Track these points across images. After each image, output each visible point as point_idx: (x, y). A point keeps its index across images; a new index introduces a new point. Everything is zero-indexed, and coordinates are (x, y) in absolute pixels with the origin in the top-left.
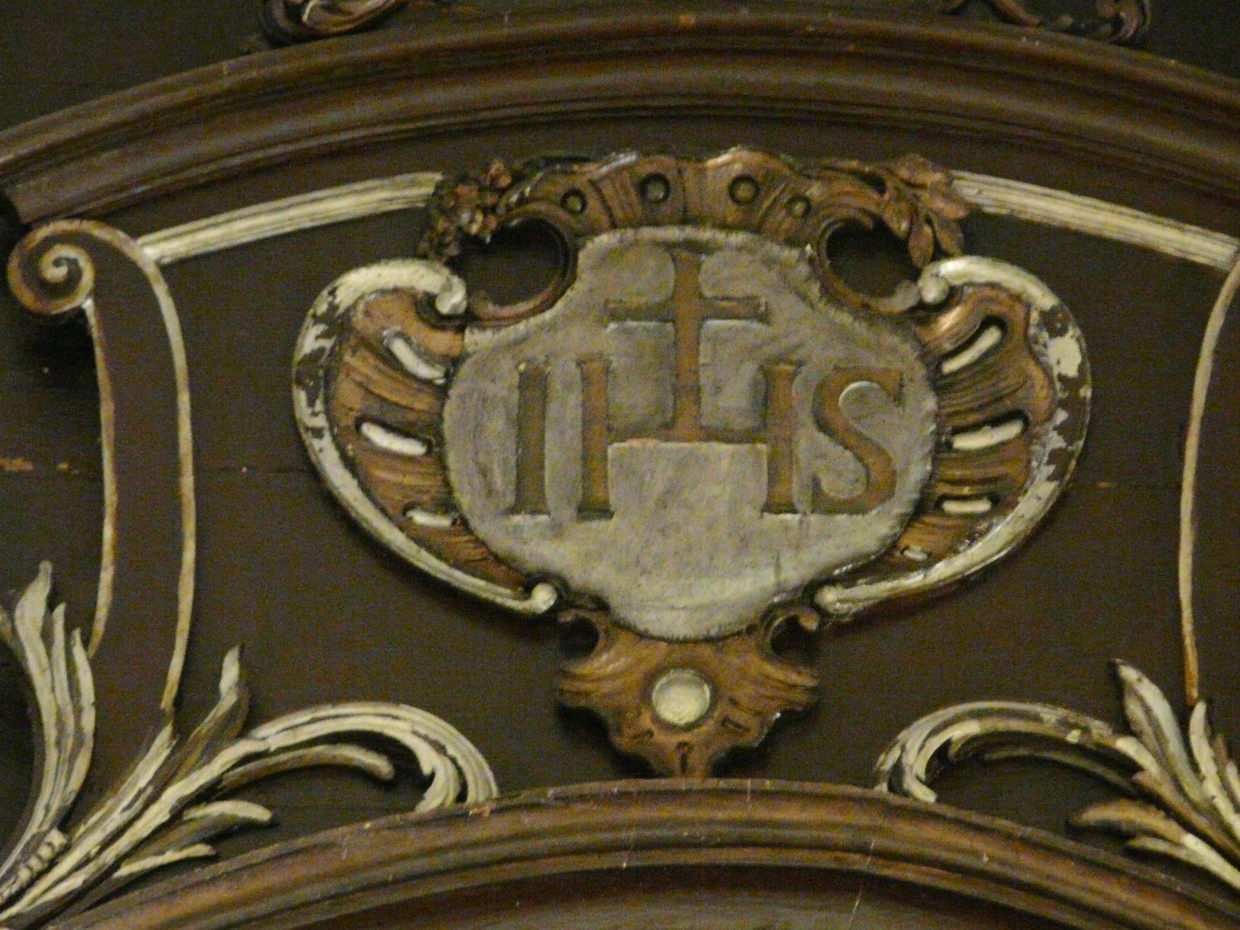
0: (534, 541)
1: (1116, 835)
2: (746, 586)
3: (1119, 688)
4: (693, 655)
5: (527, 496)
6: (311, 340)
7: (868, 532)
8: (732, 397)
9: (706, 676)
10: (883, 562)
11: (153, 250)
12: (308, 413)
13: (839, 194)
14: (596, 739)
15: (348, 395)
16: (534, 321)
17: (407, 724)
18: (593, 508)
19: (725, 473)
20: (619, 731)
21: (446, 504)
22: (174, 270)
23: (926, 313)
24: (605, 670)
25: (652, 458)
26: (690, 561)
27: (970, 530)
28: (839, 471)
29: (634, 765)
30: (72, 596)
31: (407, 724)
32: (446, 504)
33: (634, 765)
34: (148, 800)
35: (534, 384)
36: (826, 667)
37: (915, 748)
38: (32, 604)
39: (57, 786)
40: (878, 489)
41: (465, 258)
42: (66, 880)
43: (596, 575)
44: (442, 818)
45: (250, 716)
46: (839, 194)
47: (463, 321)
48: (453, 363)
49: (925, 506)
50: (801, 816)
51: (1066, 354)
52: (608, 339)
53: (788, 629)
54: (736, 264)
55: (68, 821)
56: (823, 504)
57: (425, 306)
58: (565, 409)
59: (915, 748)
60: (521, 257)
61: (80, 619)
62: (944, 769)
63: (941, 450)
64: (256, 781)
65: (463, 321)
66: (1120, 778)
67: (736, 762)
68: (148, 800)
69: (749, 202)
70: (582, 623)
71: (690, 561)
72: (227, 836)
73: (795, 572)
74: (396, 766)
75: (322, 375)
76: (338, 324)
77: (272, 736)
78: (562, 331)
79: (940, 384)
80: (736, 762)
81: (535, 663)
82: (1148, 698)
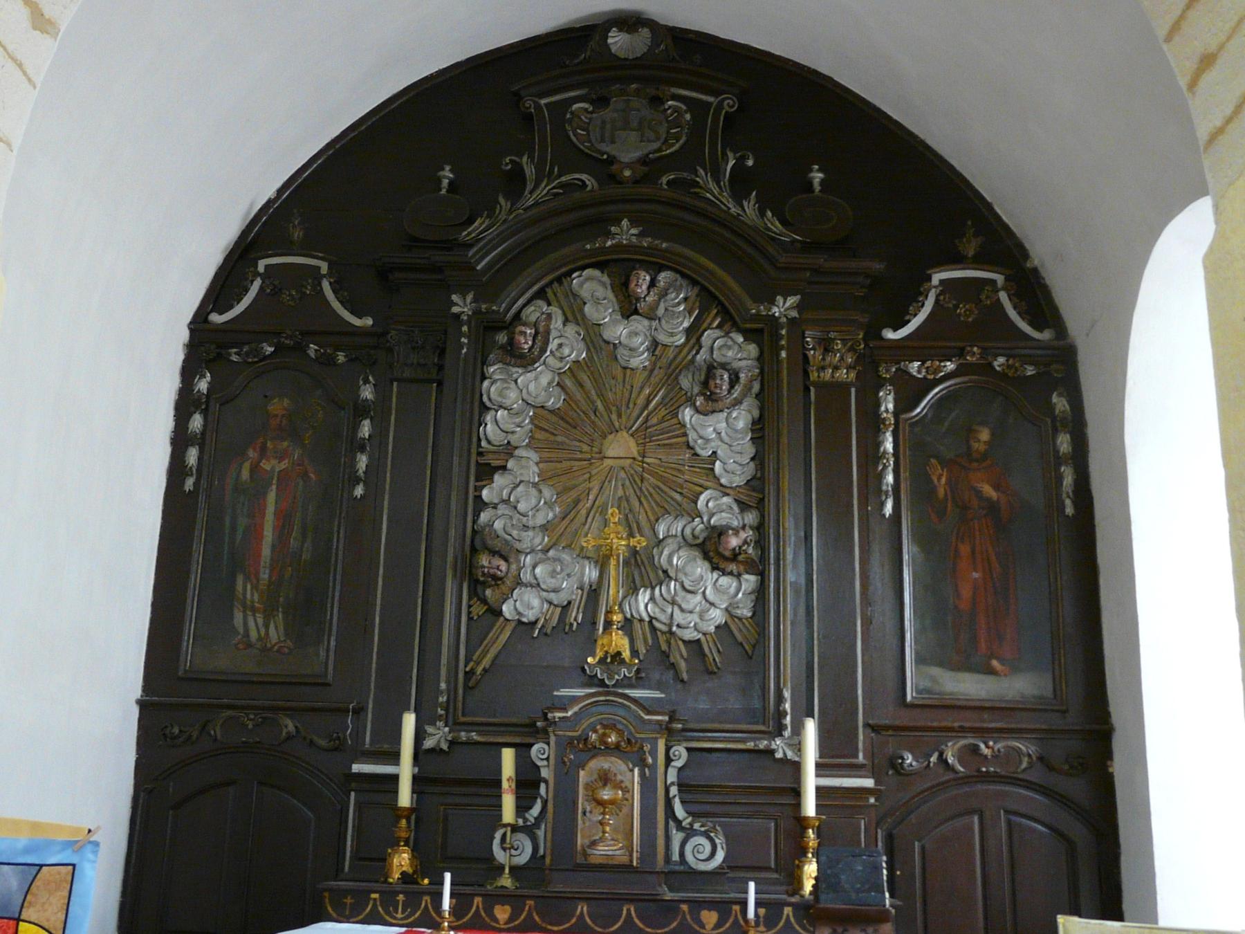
0: (604, 147)
1: (696, 193)
2: (637, 154)
3: (696, 171)
4: (628, 166)
5: (603, 141)
6: (568, 116)
7: (656, 146)
8: (635, 124)
9: (631, 168)
10: (659, 150)
11: (543, 102)
12: (568, 127)
13: (651, 91)
14: (614, 179)
15: (575, 125)
16: (609, 257)
17: (584, 177)
18: (613, 142)
19: (633, 136)
20: (502, 371)
21: (590, 141)
22: (546, 105)
23: (666, 110)
24: (614, 167)
25: (623, 134)
26: (628, 151)
27: (673, 145)
28: (652, 135)
29: (620, 183)
30: (531, 157)
31: (584, 177)
32: (590, 141)
33: (620, 183)
34: (544, 190)
35: (604, 122)
36: (651, 167)
37: (664, 180)
38: (525, 159)
39: (529, 187)
40: (658, 139)
41: (592, 102)
42: (531, 202)
43: (613, 153)
44: (592, 191)
45: (560, 176)
46: (651, 91)
47: (592, 113)
48: (590, 119)
49: (666, 141)
50: (645, 190)
51: (688, 117)
52: (616, 115)
53: (644, 161)
54: (635, 102)
55: (531, 193)
56: (649, 141)
57: (586, 110)
58: (608, 126)
59: (664, 180)
60: (601, 102)
61: (532, 161)
62: (669, 183)
63: (668, 132)
64: (561, 186)
65: (592, 113)
66: (697, 184)
67: (636, 182)
68: (544, 190)
69: (637, 92)
70: (612, 160)
71: (628, 151)
72: (556, 195)
73: (645, 152)
74: (882, 339)
75: (570, 121)
76: (572, 113)
77: (563, 179)
78: (608, 114)
79: (668, 122)
80: (636, 182)
81: (605, 168)
82: (702, 172)
